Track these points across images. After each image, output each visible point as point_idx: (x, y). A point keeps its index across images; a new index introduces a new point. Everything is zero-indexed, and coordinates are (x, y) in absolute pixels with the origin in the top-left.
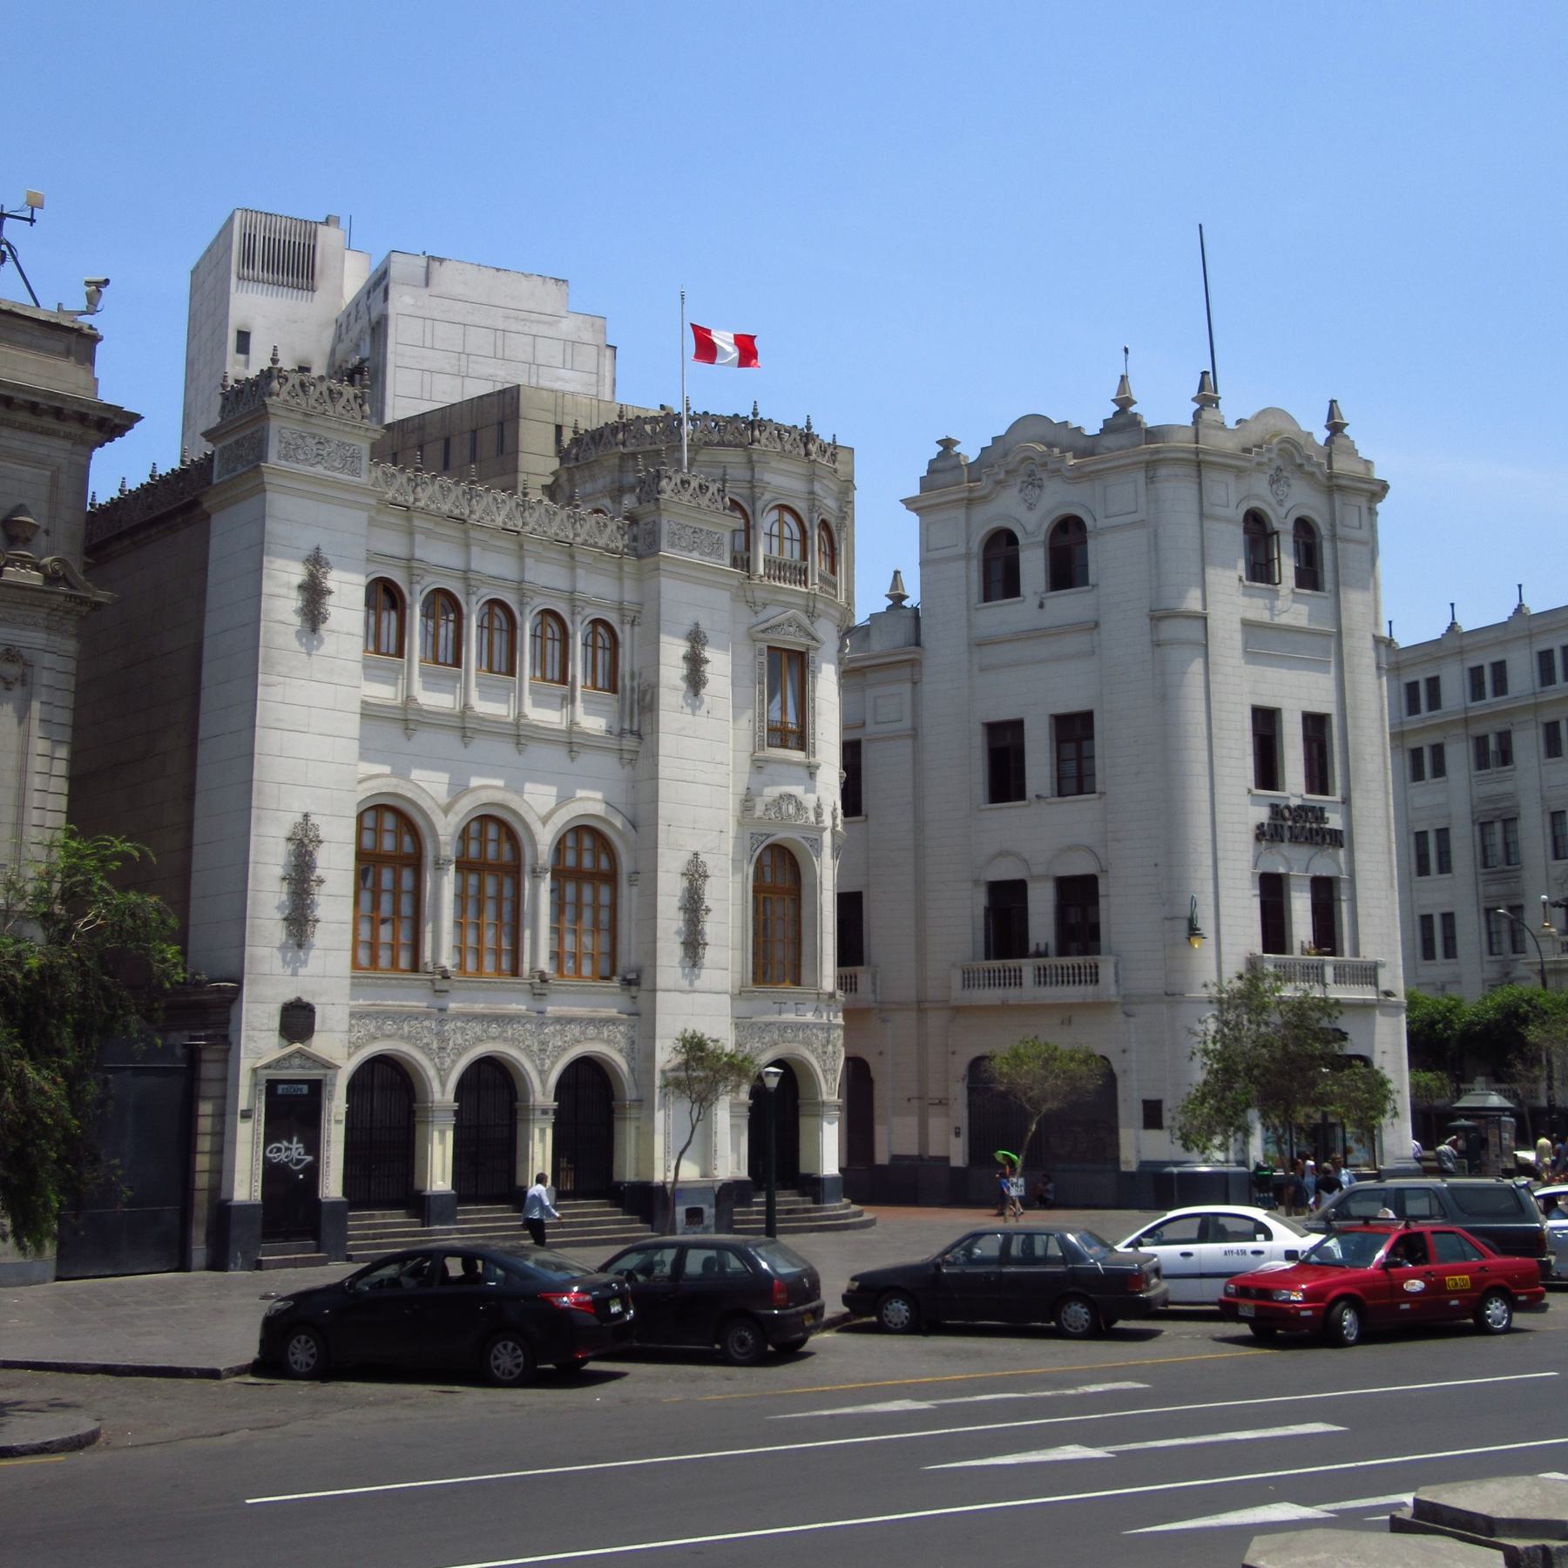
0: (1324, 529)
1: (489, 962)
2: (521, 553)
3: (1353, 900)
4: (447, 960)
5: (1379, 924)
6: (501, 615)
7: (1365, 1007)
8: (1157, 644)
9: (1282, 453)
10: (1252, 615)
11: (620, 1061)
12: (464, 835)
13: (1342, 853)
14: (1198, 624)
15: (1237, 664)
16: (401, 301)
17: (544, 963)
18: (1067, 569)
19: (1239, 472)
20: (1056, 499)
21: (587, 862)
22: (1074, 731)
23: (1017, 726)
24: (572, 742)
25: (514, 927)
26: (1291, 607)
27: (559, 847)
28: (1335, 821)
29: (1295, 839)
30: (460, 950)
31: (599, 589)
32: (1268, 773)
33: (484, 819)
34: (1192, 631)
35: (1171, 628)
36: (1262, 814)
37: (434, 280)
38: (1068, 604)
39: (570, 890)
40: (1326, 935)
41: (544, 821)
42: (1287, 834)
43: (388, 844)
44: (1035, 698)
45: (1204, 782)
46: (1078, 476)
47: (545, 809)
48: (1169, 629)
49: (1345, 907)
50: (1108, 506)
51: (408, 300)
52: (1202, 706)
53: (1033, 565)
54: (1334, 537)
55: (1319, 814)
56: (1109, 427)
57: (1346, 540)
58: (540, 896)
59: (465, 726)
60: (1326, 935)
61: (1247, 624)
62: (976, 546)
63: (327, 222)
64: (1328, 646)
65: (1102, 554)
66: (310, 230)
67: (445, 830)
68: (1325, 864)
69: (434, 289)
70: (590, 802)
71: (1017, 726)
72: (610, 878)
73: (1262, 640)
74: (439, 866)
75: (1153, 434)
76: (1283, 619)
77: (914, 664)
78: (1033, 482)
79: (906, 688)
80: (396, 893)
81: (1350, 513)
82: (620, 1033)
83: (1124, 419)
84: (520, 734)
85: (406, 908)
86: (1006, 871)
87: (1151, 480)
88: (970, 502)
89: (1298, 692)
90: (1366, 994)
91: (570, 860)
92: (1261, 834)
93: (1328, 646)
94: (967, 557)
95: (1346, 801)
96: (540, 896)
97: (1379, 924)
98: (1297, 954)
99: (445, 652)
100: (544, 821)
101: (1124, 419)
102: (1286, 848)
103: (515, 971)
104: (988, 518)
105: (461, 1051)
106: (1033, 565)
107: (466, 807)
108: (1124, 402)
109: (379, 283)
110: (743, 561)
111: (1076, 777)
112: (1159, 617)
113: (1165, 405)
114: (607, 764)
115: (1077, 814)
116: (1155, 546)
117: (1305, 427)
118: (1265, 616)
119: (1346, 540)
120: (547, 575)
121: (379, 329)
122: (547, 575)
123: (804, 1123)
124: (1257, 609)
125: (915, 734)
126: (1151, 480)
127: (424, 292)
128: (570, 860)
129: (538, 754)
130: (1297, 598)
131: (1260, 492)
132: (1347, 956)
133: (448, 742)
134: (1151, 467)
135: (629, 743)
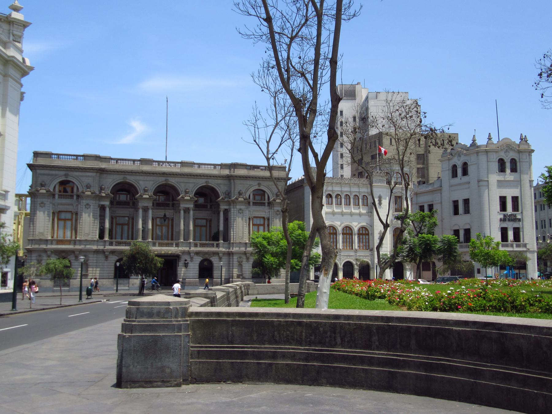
0: (518, 160)
1: (348, 248)
2: (350, 187)
3: (523, 231)
4: (341, 248)
5: (530, 236)
6: (347, 197)
7: (526, 251)
8: (479, 186)
9: (508, 146)
10: (499, 179)
11: (370, 262)
12: (343, 229)
13: (521, 223)
14: (487, 182)
15: (495, 187)
16: (371, 103)
17: (357, 247)
18: (465, 172)
19: (496, 152)
20: (463, 159)
21: (364, 232)
22: (466, 202)
23: (458, 201)
24: (360, 215)
25: (352, 243)
26: (509, 176)
27: (359, 230)
28: (519, 217)
29: (509, 220)
30: (343, 246)
31: (365, 190)
32: (503, 207)
33: (346, 227)
34: (485, 183)
35: (482, 183)
36: (502, 217)
37: (378, 97)
38: (465, 179)
39: (361, 236)
40: (517, 238)
41: (356, 227)
42: (507, 220)
43: (331, 231)
44: (460, 196)
45: (488, 211)
46: (466, 155)
47: (356, 226)
48: (481, 183)
49: (521, 233)
50: (471, 160)
51: (372, 103)
52: (487, 197)
53: (460, 171)
54: (520, 162)
55: (515, 216)
56: (471, 145)
57: (522, 162)
58: (356, 238)
59: (342, 214)
60: (517, 238)
61: (498, 181)
62: (450, 168)
63: (358, 84)
64: (519, 183)
65: (470, 169)
66: (354, 86)
67: (340, 229)
68: (516, 225)
69: (378, 99)
70: (364, 224)
71: (458, 201)
72: (368, 234)
73: (501, 184)
74: (339, 234)
75: (478, 147)
76: (507, 179)
77: (441, 190)
78: (459, 156)
79: (439, 194)
80: (333, 238)
81: (524, 156)
82: (369, 258)
83: (474, 144)
84: (351, 214)
85: (335, 240)
86: (456, 228)
87: (477, 155)
88: (449, 160)
89: (510, 193)
90: (525, 249)
91: (361, 232)
92: (501, 220)
93: (519, 183)
94: (449, 170)
95: (522, 213)
96: (356, 238)
97: (530, 236)
98: (509, 242)
99: (339, 202)
100: (356, 227)
101: (474, 144)
102: (507, 222)
103: (352, 249)
104: (452, 162)
105: (343, 260)
106: (460, 171)
107: (343, 225)
108: (474, 141)
109: (367, 98)
110: (389, 183)
111: (467, 211)
112: (479, 181)
113: (481, 141)
114: (366, 217)
115: (467, 217)
116: (478, 168)
117: (513, 140)
118: (503, 179)
119: (522, 162)
120: (355, 189)
121: (367, 109)
122: (355, 189)
123: (404, 271)
124: (501, 177)
125: (441, 203)
126: (477, 155)
127: (376, 100)
128: (361, 232)
129: (354, 217)
130: (510, 175)
131: (502, 155)
132: (522, 242)
133: (340, 216)
134: (477, 153)
135: (370, 214)
